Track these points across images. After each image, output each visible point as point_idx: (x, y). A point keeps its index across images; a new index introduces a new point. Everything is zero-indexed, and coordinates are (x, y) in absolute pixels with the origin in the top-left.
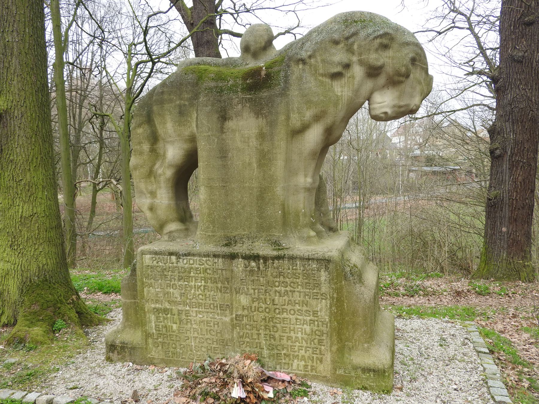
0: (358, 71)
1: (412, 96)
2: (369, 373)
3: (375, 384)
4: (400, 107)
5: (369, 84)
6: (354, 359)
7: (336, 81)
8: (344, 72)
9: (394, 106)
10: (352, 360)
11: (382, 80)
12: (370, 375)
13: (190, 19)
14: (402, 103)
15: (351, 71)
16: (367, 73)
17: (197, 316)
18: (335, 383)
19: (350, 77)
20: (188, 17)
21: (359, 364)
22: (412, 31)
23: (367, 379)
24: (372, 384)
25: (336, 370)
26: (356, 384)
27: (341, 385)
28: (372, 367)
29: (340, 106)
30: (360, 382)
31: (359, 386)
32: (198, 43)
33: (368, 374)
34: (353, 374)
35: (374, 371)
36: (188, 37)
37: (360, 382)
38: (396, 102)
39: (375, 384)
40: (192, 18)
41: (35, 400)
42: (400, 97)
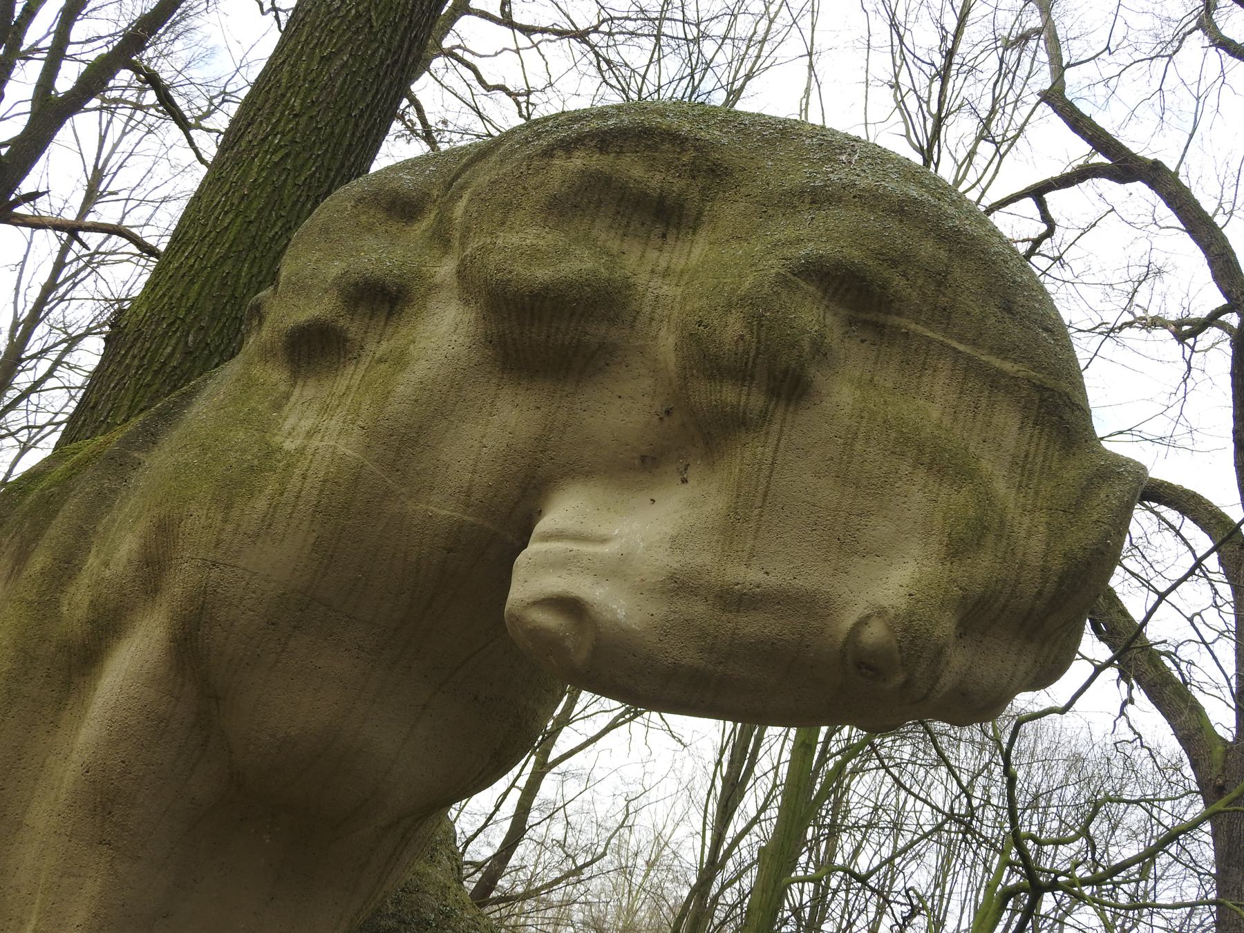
0: (443, 331)
1: (845, 542)
4: (735, 600)
5: (505, 421)
7: (312, 382)
8: (353, 329)
9: (679, 586)
11: (619, 409)
13: (1216, 770)
14: (750, 576)
15: (404, 331)
16: (489, 341)
19: (380, 361)
20: (1211, 767)
22: (1199, 337)
29: (261, 504)
32: (1229, 854)
36: (1195, 824)
38: (702, 558)
40: (1224, 769)
42: (734, 527)
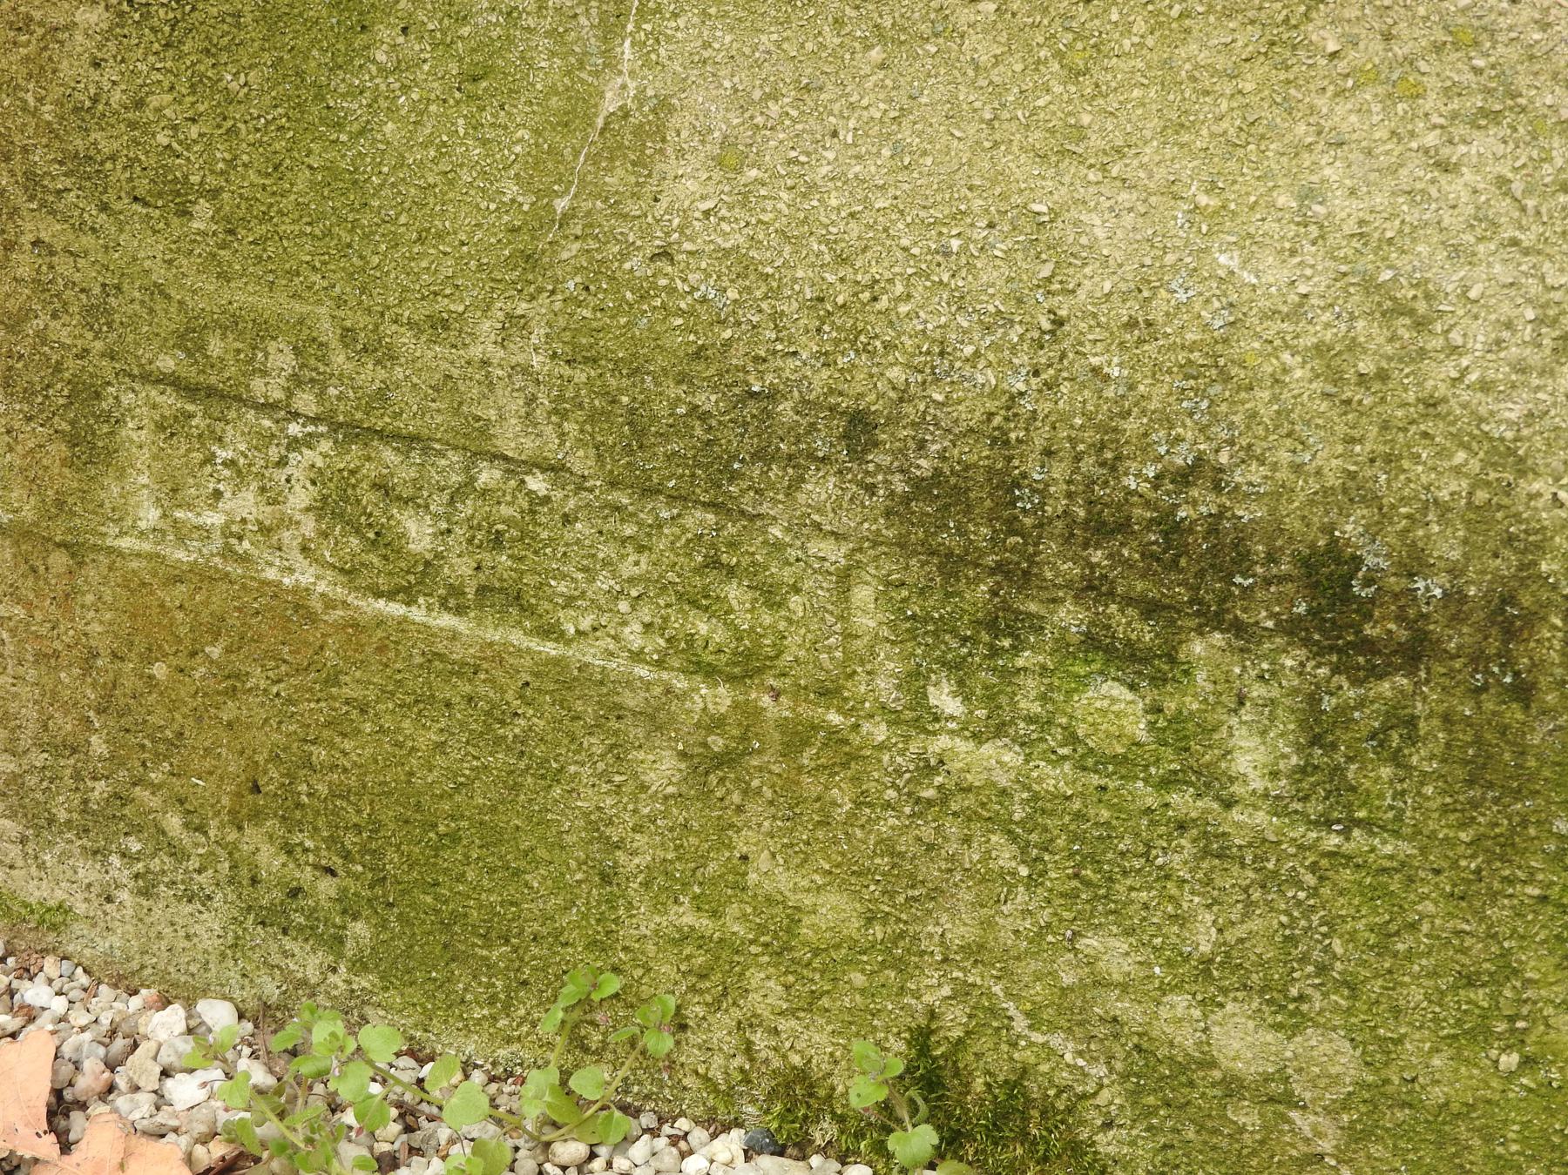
2: (1152, 666)
3: (1330, 1055)
6: (708, 108)
10: (641, 138)
12: (1187, 752)
17: (721, 742)
18: (100, 826)
21: (847, 323)
23: (1087, 863)
24: (1241, 1040)
25: (91, 448)
26: (717, 973)
27: (280, 913)
28: (1291, 466)
30: (832, 912)
31: (813, 1043)
33: (1113, 707)
34: (614, 638)
35: (1337, 606)
37: (832, 912)
39: (1330, 1055)
41: (36, 1161)
